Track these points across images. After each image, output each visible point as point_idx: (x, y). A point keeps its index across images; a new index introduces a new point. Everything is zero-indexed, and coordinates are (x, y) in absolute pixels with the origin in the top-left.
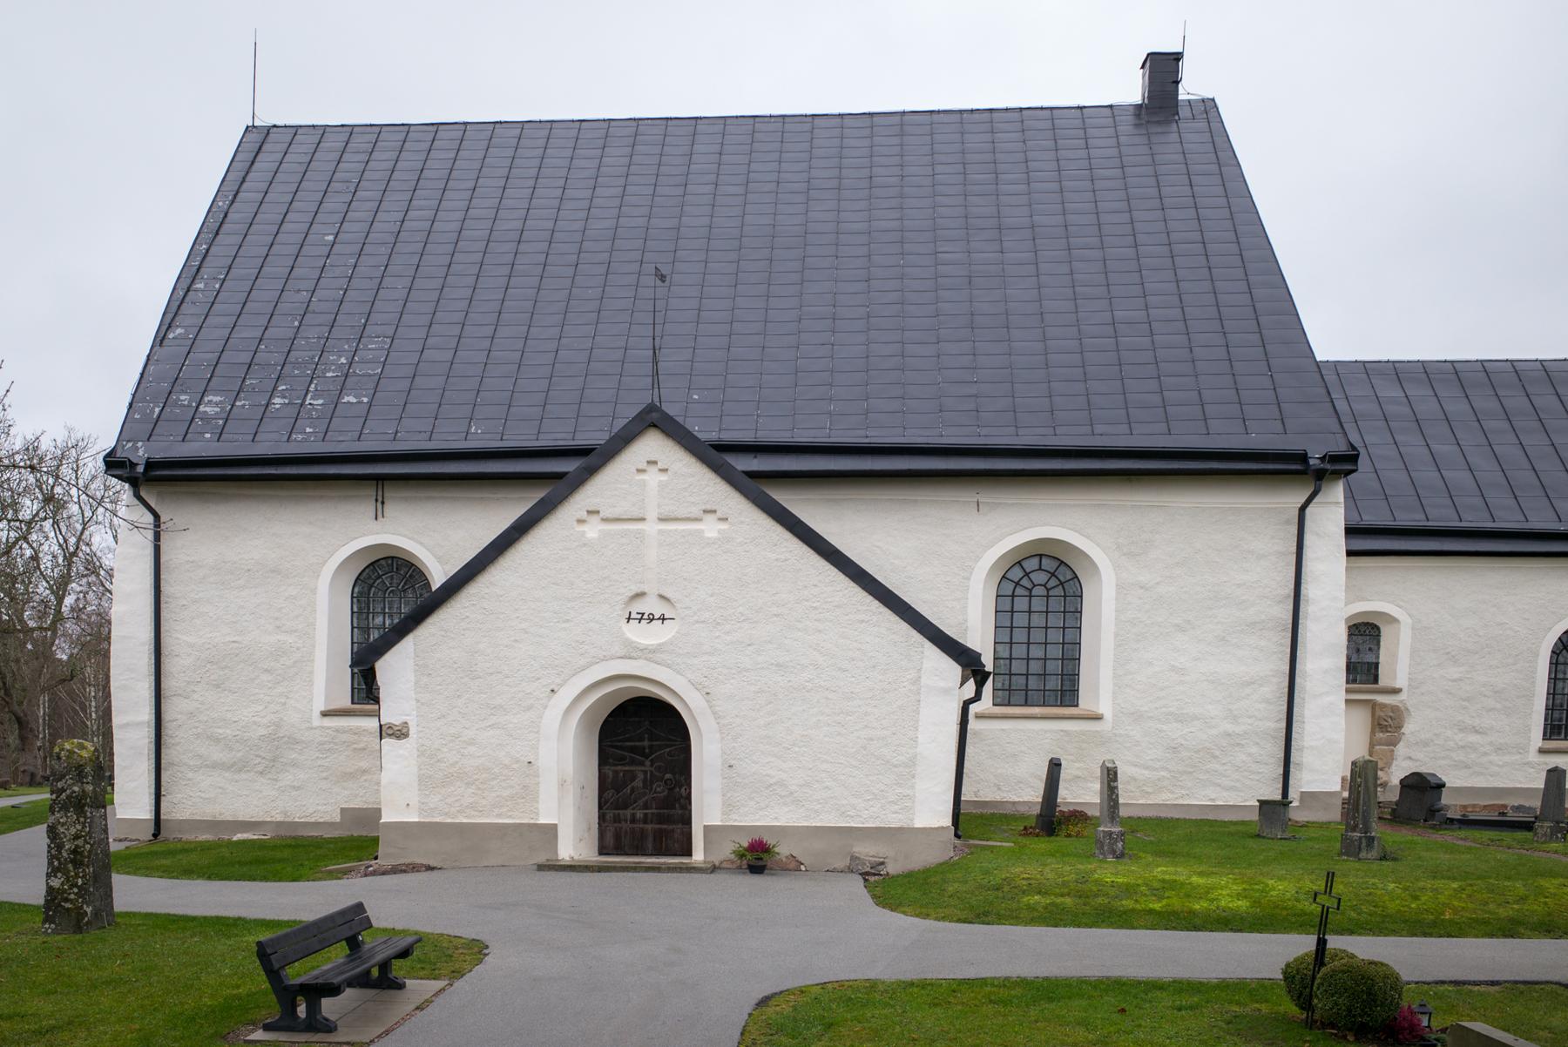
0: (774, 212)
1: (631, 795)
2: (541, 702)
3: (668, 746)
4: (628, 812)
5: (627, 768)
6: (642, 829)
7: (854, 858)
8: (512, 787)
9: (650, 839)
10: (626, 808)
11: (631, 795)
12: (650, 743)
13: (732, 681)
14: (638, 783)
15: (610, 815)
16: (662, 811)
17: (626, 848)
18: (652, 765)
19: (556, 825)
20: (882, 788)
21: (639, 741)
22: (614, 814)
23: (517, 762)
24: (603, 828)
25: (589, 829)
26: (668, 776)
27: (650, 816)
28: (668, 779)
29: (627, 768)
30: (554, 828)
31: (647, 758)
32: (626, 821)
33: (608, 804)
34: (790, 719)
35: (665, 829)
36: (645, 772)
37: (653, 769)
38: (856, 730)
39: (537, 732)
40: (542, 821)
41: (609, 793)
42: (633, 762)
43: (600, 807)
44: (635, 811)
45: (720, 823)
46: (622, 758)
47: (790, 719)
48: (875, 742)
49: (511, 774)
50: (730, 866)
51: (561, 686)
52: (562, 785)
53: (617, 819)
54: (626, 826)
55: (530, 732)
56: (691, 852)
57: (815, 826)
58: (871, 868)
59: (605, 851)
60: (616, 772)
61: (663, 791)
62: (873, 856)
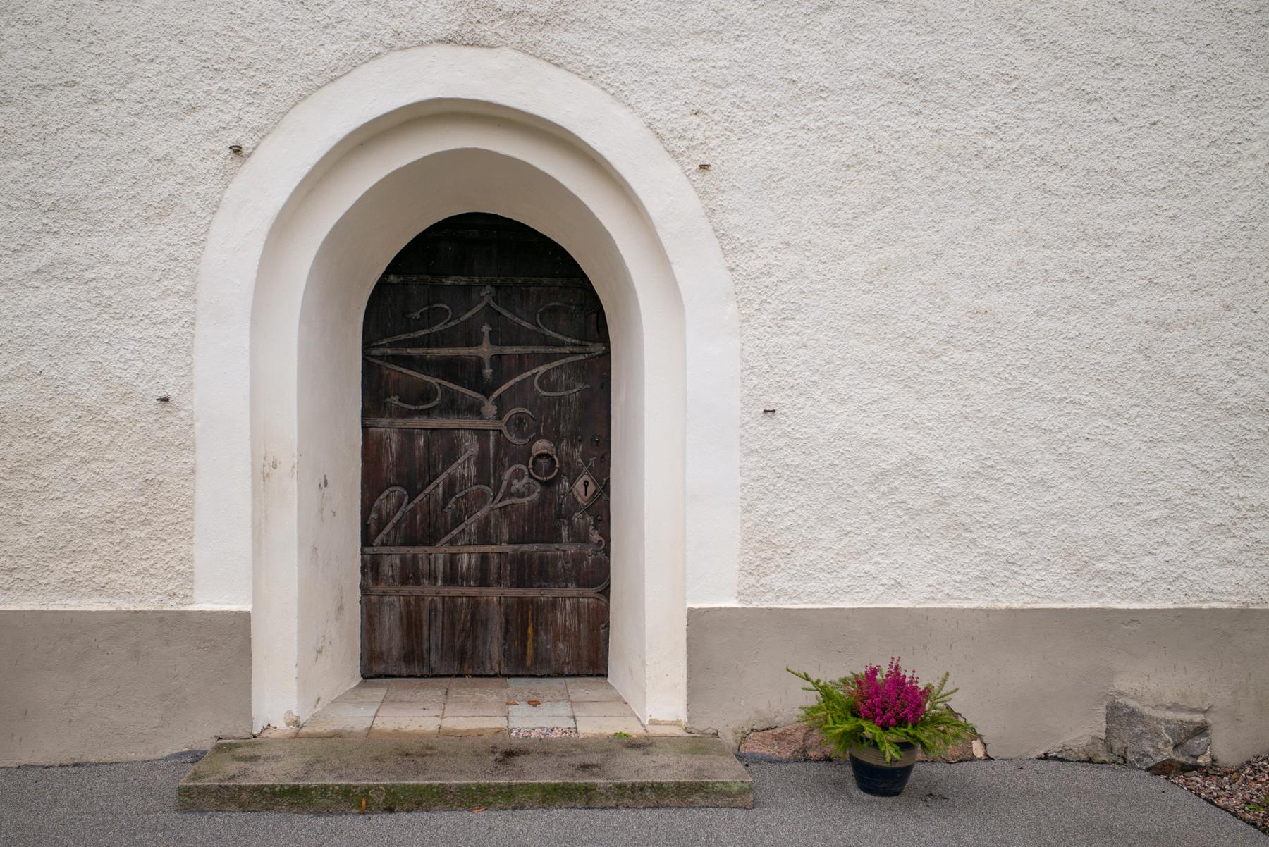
2: (200, 189)
3: (548, 358)
4: (439, 553)
5: (433, 423)
7: (1118, 715)
8: (109, 485)
9: (496, 628)
10: (432, 540)
12: (497, 350)
13: (772, 129)
14: (464, 467)
15: (391, 561)
16: (525, 548)
17: (434, 658)
18: (499, 416)
19: (248, 614)
20: (1193, 483)
21: (469, 344)
22: (403, 560)
23: (125, 398)
24: (374, 599)
25: (340, 609)
26: (542, 446)
27: (494, 562)
28: (541, 456)
29: (433, 423)
30: (239, 626)
31: (488, 396)
32: (433, 577)
33: (388, 528)
34: (939, 255)
35: (532, 600)
36: (482, 434)
37: (501, 425)
38: (1123, 295)
39: (187, 295)
40: (205, 603)
41: (390, 498)
42: (452, 406)
43: (366, 540)
44: (454, 550)
45: (734, 604)
46: (426, 395)
47: (939, 255)
48: (1178, 333)
49: (105, 439)
50: (772, 751)
51: (262, 133)
52: (266, 477)
53: (410, 573)
54: (433, 592)
55: (166, 293)
56: (604, 662)
57: (1011, 611)
58: (1176, 747)
59: (379, 668)
60: (408, 435)
61: (530, 491)
62: (1174, 707)
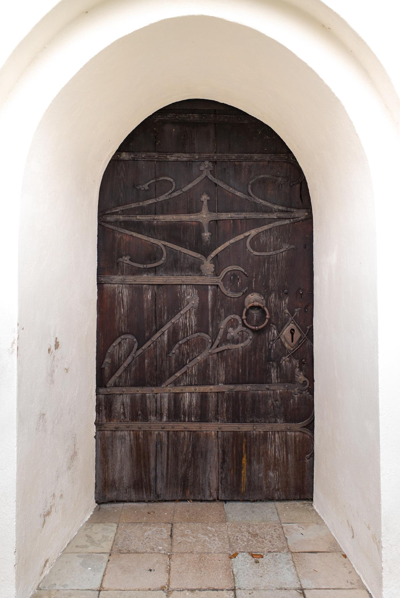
0: (163, 582)
1: (170, 347)
3: (258, 223)
5: (160, 279)
6: (196, 436)
10: (158, 381)
11: (170, 347)
12: (214, 216)
16: (239, 388)
18: (216, 273)
21: (190, 212)
22: (133, 399)
24: (108, 433)
27: (212, 400)
29: (160, 279)
31: (206, 256)
32: (159, 414)
36: (202, 289)
37: (218, 280)
43: (101, 382)
44: (177, 390)
61: (243, 339)
